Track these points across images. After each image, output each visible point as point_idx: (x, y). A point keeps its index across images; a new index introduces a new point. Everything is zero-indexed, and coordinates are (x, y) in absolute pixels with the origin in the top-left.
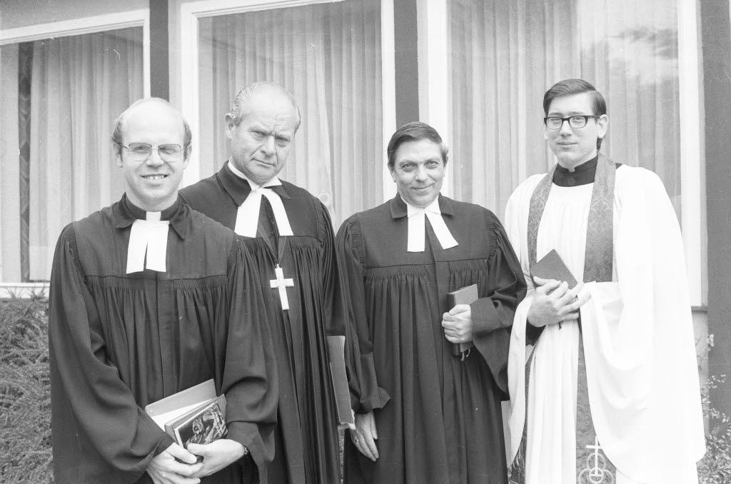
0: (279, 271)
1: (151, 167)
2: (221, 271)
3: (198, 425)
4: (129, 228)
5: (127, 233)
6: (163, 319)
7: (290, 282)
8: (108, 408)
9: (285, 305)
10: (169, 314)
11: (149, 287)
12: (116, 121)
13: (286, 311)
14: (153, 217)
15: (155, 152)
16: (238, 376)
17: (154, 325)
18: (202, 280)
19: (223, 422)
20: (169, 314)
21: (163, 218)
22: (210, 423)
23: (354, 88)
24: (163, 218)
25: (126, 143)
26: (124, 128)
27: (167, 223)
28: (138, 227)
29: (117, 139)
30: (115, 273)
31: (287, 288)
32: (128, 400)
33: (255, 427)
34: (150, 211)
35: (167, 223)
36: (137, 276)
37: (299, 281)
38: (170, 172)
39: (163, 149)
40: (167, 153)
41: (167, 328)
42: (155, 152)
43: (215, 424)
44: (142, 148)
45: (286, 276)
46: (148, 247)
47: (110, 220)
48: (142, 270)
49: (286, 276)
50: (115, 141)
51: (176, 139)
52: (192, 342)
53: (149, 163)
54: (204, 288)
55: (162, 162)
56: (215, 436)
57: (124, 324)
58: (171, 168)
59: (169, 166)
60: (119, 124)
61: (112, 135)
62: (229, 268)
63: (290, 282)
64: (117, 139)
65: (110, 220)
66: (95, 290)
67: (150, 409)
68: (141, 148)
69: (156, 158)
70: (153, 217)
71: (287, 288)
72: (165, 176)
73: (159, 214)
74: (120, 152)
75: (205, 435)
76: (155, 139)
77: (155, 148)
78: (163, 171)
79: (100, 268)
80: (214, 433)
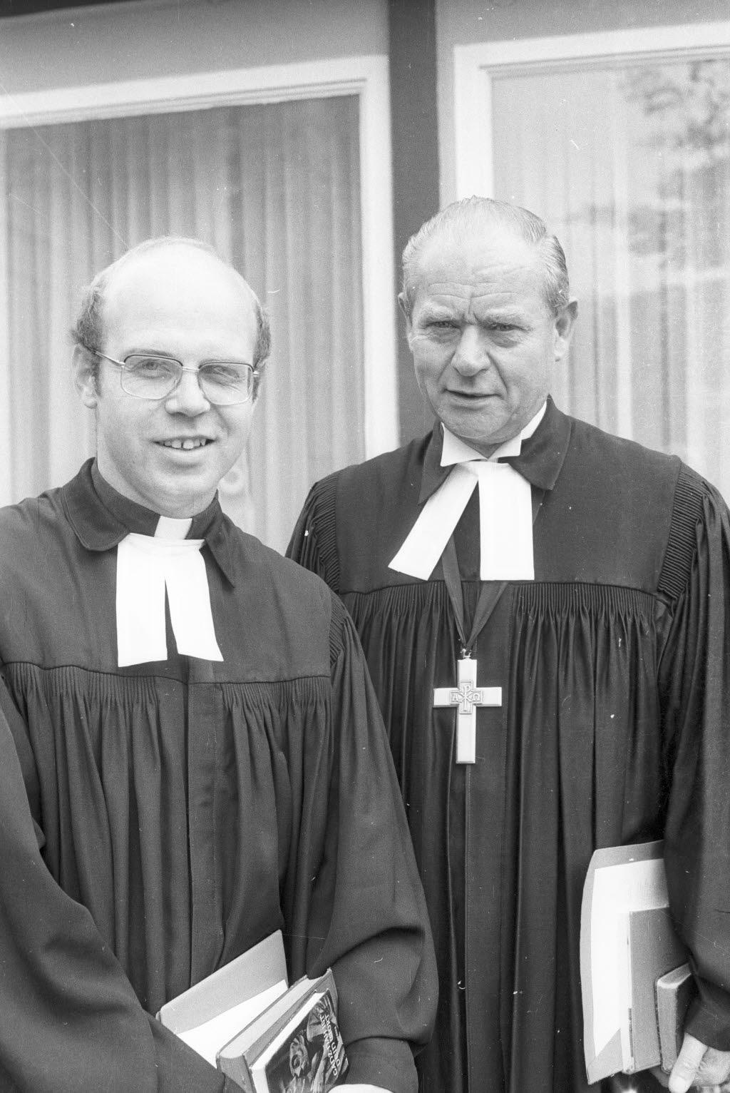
0: (468, 668)
1: (181, 416)
2: (323, 668)
3: (299, 1053)
4: (113, 551)
5: (108, 560)
6: (198, 780)
7: (493, 696)
8: (61, 1009)
9: (466, 751)
10: (210, 769)
11: (169, 695)
12: (86, 290)
13: (463, 766)
14: (173, 529)
15: (190, 380)
16: (377, 923)
17: (177, 794)
18: (282, 685)
19: (340, 1039)
20: (210, 769)
21: (191, 535)
22: (315, 1046)
23: (290, 244)
24: (191, 535)
25: (113, 349)
26: (108, 310)
27: (199, 543)
28: (133, 555)
29: (89, 339)
30: (83, 659)
31: (482, 711)
32: (118, 989)
33: (405, 1048)
34: (164, 516)
35: (199, 543)
36: (143, 672)
37: (515, 697)
38: (223, 435)
39: (209, 371)
40: (219, 383)
41: (206, 804)
42: (190, 380)
43: (326, 1047)
44: (153, 364)
45: (484, 679)
46: (160, 602)
47: (53, 527)
48: (161, 655)
49: (484, 679)
50: (81, 341)
51: (239, 349)
52: (262, 844)
53: (173, 405)
54: (285, 703)
55: (207, 406)
56: (328, 1075)
57: (104, 792)
58: (226, 425)
59: (220, 415)
60: (96, 298)
61: (75, 326)
62: (333, 661)
63: (493, 696)
64: (89, 339)
65: (53, 527)
66: (31, 700)
67: (170, 1014)
68: (150, 365)
69: (192, 394)
70: (173, 529)
71: (482, 711)
72: (209, 441)
73: (185, 524)
74: (95, 370)
75: (310, 1075)
76: (190, 342)
77: (191, 366)
78: (207, 428)
79: (44, 645)
80: (325, 1071)
